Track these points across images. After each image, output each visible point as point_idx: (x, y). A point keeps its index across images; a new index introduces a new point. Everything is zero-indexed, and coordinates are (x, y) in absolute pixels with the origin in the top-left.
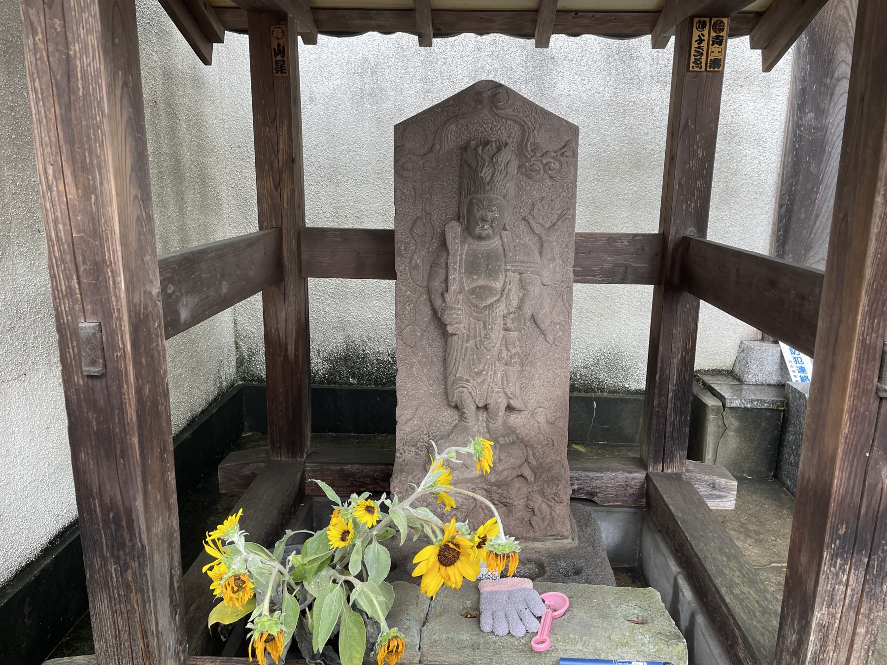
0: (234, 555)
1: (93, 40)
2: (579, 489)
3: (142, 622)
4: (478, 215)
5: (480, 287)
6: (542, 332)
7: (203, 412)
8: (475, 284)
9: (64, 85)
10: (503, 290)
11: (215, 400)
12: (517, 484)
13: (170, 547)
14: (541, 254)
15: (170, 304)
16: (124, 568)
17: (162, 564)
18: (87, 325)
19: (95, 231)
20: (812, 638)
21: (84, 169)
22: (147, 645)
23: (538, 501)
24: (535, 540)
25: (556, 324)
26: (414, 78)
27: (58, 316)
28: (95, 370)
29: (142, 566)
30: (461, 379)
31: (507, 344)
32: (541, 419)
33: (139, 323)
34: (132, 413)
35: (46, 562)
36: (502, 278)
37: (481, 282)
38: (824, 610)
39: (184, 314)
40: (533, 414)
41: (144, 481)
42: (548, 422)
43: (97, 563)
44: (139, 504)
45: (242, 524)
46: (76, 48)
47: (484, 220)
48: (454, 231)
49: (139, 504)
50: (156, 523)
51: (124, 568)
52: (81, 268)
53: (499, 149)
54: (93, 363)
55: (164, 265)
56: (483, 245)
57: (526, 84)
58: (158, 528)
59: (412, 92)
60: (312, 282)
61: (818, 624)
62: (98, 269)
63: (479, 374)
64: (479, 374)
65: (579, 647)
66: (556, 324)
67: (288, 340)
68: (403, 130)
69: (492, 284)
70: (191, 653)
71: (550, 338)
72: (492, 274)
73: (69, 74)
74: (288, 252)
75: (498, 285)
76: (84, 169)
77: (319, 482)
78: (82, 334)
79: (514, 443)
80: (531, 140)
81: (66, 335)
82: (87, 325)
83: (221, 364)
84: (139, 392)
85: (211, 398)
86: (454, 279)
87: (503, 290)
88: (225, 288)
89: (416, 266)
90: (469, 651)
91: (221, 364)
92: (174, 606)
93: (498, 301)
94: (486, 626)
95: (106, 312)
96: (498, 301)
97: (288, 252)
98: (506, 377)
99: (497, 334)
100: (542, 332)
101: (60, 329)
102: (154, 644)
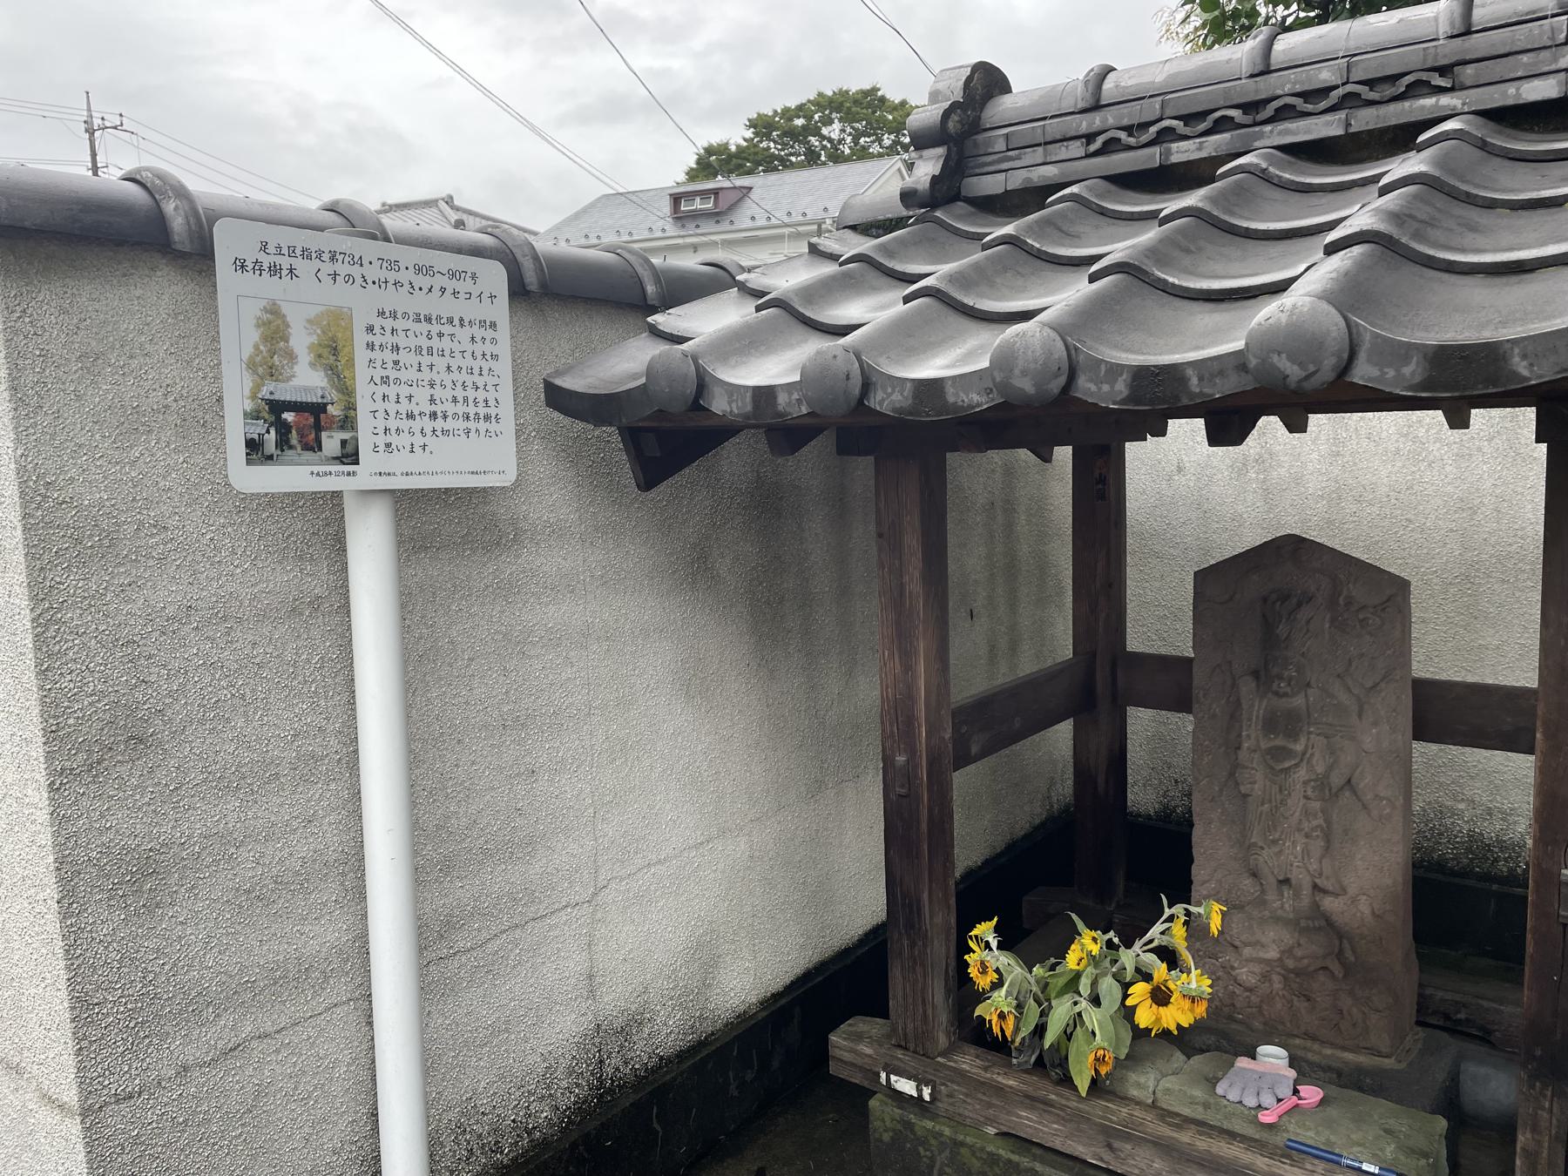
0: (987, 954)
1: (917, 574)
2: (1467, 1020)
3: (924, 990)
4: (1275, 671)
5: (1277, 748)
6: (1365, 807)
7: (1025, 837)
8: (1272, 744)
9: (897, 601)
10: (1304, 754)
11: (1042, 824)
12: (1322, 977)
13: (948, 939)
14: (1360, 716)
15: (961, 742)
16: (913, 945)
17: (940, 949)
18: (901, 759)
19: (910, 696)
20: (1518, 1162)
21: (906, 656)
22: (925, 1012)
23: (1346, 1002)
24: (1344, 1048)
25: (1382, 799)
26: (1316, 438)
27: (884, 750)
28: (903, 791)
29: (925, 946)
30: (1255, 844)
31: (1307, 813)
32: (1364, 907)
33: (933, 762)
34: (924, 826)
35: (860, 952)
36: (1303, 741)
37: (1279, 742)
38: (1529, 1135)
39: (974, 750)
40: (1354, 900)
41: (930, 881)
42: (1373, 913)
43: (896, 936)
44: (925, 896)
45: (997, 929)
46: (906, 579)
47: (1280, 678)
48: (1247, 687)
49: (925, 896)
50: (938, 917)
51: (913, 945)
52: (898, 719)
53: (1299, 605)
54: (902, 786)
55: (955, 714)
56: (1284, 703)
57: (1490, 440)
58: (939, 919)
59: (1315, 456)
60: (1131, 710)
61: (1523, 1149)
62: (910, 721)
63: (1275, 842)
64: (1275, 842)
65: (1311, 1134)
66: (1382, 799)
67: (1103, 770)
68: (1204, 578)
69: (1291, 746)
70: (960, 1039)
71: (1375, 813)
72: (1293, 735)
73: (902, 594)
74: (1104, 678)
75: (1299, 747)
76: (906, 656)
77: (1074, 916)
78: (898, 764)
79: (1320, 928)
80: (1345, 593)
81: (888, 761)
82: (901, 759)
83: (1052, 782)
84: (930, 810)
85: (1037, 822)
86: (1248, 736)
87: (1304, 754)
88: (1017, 723)
89: (1214, 716)
90: (1200, 1109)
91: (1052, 782)
92: (948, 991)
93: (1297, 765)
94: (1220, 1090)
95: (912, 752)
96: (1297, 765)
97: (1104, 678)
98: (1306, 852)
99: (1295, 804)
100: (1365, 807)
101: (884, 760)
102: (930, 1012)
